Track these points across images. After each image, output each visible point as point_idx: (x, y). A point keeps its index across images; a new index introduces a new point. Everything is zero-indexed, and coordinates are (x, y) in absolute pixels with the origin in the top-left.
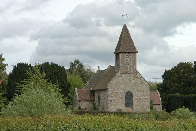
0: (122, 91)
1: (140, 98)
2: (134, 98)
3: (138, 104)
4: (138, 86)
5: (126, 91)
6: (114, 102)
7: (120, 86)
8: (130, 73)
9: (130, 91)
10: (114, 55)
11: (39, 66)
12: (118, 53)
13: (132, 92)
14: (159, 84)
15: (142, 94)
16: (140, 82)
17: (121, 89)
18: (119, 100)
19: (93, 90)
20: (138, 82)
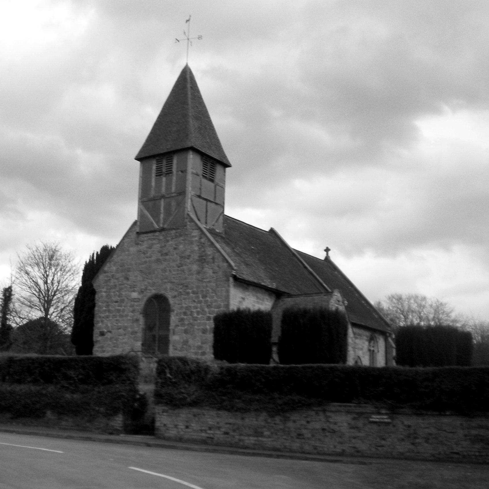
0: (135, 295)
1: (195, 319)
2: (174, 319)
3: (186, 342)
4: (190, 270)
5: (149, 294)
6: (109, 335)
7: (132, 278)
8: (165, 226)
9: (162, 292)
10: (138, 163)
11: (144, 398)
12: (169, 155)
13: (169, 295)
14: (110, 248)
15: (200, 302)
16: (196, 256)
17: (133, 288)
18: (125, 329)
19: (295, 416)
20: (189, 256)
